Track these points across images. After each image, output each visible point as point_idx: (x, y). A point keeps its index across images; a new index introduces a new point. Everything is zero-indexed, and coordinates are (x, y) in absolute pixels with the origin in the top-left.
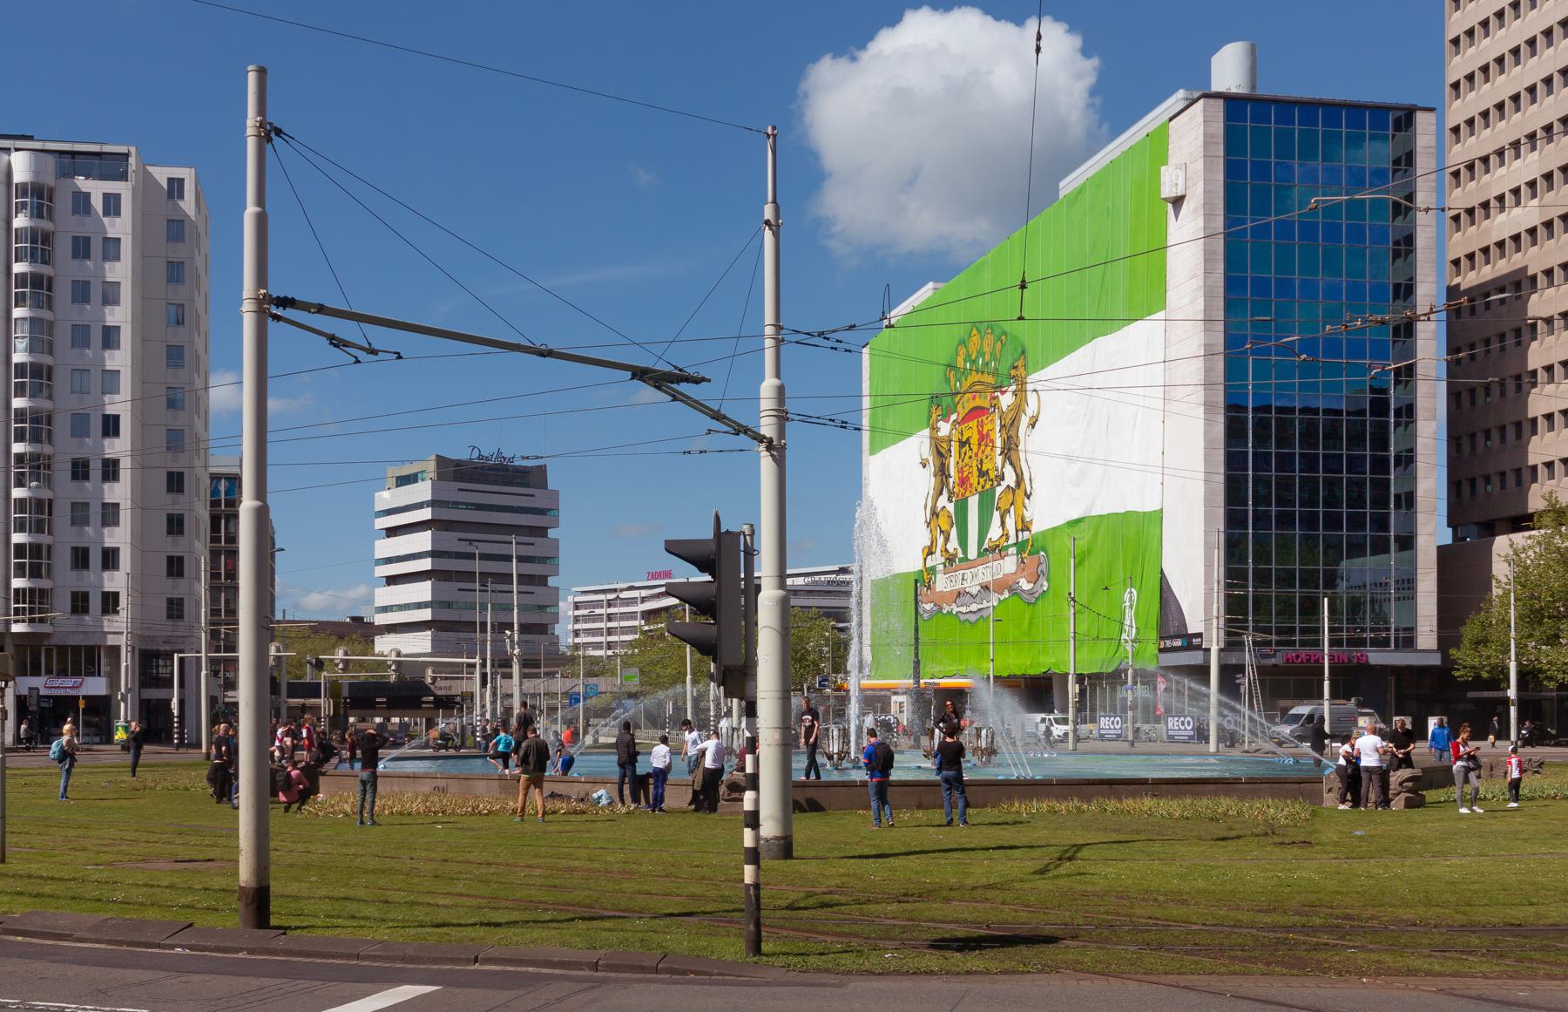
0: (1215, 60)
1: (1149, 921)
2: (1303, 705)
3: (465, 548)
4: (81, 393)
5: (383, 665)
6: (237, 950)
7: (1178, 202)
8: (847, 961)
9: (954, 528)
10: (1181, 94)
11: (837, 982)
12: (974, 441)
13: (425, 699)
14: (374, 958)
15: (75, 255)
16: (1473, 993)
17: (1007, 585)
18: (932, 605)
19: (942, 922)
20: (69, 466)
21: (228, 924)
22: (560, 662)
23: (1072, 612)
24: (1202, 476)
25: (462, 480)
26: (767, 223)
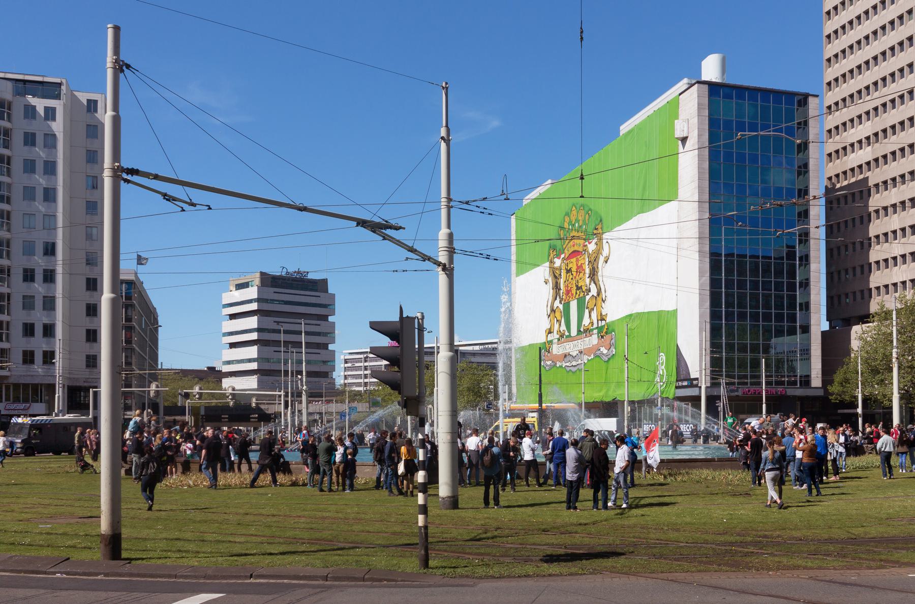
0: (704, 63)
1: (657, 541)
2: (752, 417)
3: (276, 327)
4: (29, 228)
5: (224, 396)
6: (97, 574)
7: (684, 140)
8: (480, 571)
10: (685, 81)
11: (472, 583)
12: (574, 269)
13: (252, 416)
14: (186, 577)
15: (26, 144)
16: (827, 578)
17: (595, 351)
18: (551, 362)
19: (540, 545)
20: (21, 272)
21: (95, 558)
22: (336, 394)
23: (626, 366)
24: (698, 291)
25: (276, 287)
26: (442, 138)
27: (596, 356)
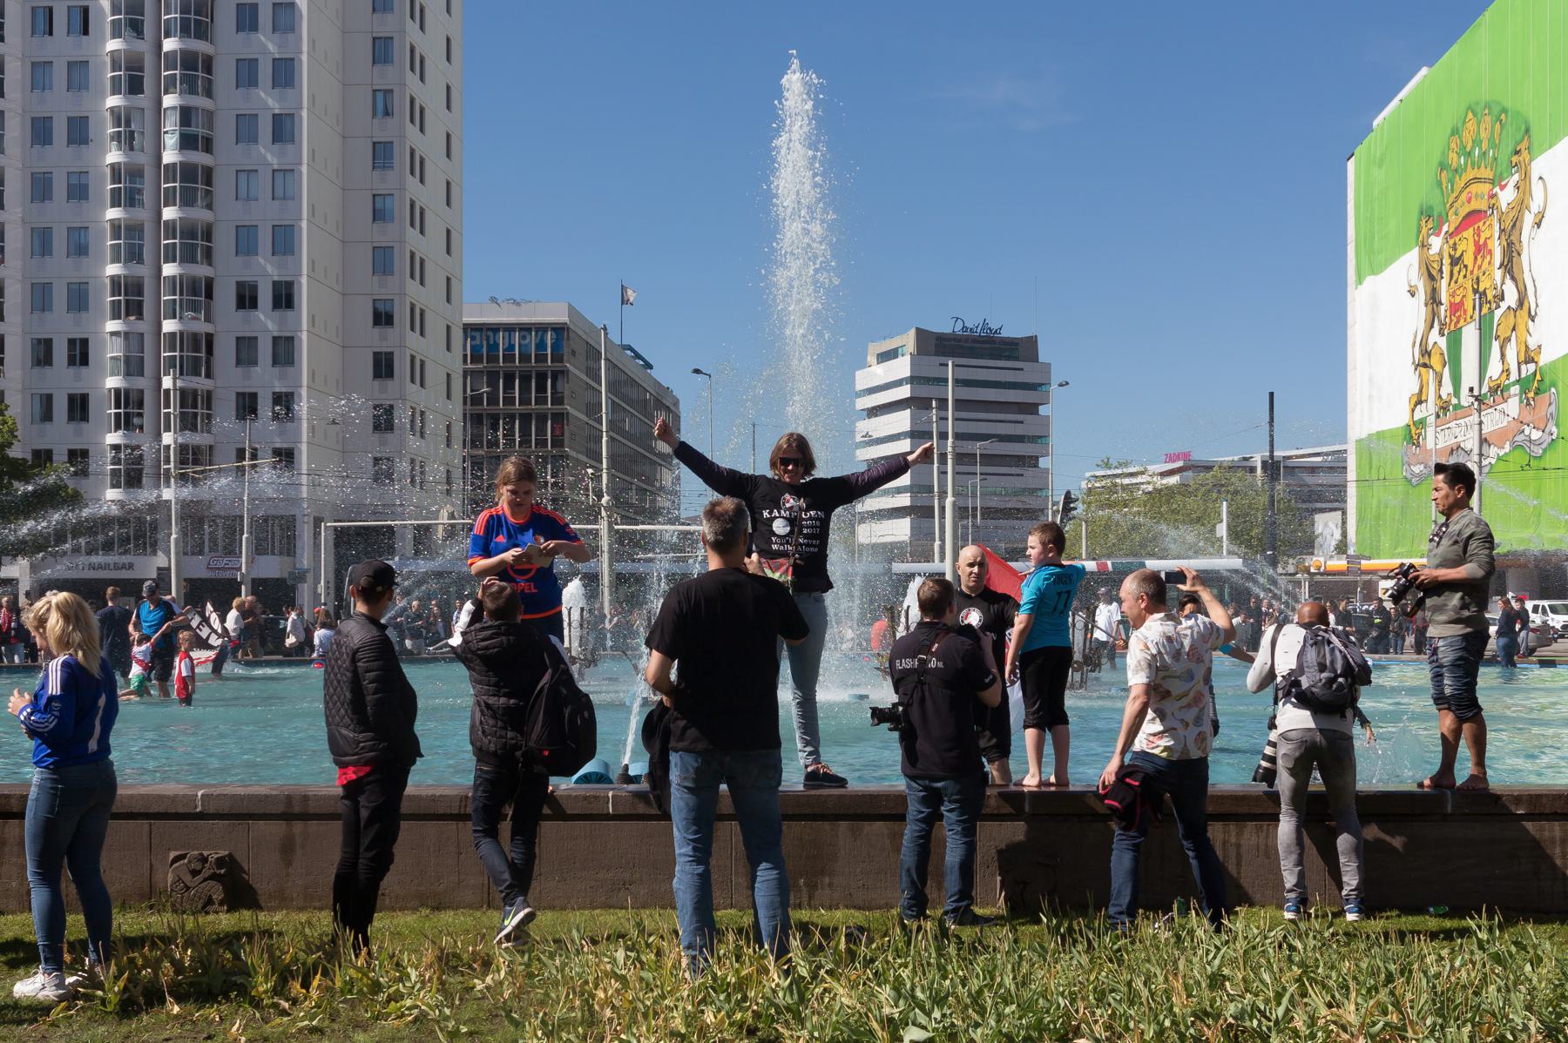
9: (1447, 369)
15: (240, 28)
18: (1422, 467)
27: (1516, 447)
